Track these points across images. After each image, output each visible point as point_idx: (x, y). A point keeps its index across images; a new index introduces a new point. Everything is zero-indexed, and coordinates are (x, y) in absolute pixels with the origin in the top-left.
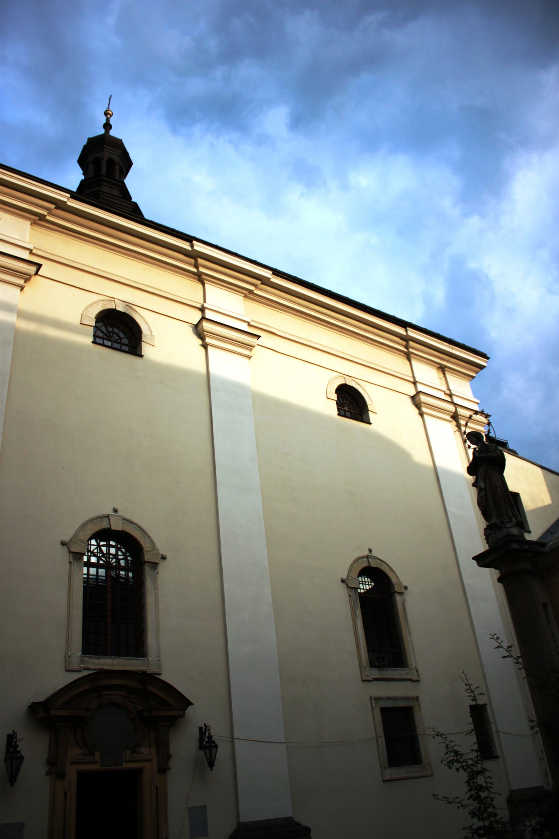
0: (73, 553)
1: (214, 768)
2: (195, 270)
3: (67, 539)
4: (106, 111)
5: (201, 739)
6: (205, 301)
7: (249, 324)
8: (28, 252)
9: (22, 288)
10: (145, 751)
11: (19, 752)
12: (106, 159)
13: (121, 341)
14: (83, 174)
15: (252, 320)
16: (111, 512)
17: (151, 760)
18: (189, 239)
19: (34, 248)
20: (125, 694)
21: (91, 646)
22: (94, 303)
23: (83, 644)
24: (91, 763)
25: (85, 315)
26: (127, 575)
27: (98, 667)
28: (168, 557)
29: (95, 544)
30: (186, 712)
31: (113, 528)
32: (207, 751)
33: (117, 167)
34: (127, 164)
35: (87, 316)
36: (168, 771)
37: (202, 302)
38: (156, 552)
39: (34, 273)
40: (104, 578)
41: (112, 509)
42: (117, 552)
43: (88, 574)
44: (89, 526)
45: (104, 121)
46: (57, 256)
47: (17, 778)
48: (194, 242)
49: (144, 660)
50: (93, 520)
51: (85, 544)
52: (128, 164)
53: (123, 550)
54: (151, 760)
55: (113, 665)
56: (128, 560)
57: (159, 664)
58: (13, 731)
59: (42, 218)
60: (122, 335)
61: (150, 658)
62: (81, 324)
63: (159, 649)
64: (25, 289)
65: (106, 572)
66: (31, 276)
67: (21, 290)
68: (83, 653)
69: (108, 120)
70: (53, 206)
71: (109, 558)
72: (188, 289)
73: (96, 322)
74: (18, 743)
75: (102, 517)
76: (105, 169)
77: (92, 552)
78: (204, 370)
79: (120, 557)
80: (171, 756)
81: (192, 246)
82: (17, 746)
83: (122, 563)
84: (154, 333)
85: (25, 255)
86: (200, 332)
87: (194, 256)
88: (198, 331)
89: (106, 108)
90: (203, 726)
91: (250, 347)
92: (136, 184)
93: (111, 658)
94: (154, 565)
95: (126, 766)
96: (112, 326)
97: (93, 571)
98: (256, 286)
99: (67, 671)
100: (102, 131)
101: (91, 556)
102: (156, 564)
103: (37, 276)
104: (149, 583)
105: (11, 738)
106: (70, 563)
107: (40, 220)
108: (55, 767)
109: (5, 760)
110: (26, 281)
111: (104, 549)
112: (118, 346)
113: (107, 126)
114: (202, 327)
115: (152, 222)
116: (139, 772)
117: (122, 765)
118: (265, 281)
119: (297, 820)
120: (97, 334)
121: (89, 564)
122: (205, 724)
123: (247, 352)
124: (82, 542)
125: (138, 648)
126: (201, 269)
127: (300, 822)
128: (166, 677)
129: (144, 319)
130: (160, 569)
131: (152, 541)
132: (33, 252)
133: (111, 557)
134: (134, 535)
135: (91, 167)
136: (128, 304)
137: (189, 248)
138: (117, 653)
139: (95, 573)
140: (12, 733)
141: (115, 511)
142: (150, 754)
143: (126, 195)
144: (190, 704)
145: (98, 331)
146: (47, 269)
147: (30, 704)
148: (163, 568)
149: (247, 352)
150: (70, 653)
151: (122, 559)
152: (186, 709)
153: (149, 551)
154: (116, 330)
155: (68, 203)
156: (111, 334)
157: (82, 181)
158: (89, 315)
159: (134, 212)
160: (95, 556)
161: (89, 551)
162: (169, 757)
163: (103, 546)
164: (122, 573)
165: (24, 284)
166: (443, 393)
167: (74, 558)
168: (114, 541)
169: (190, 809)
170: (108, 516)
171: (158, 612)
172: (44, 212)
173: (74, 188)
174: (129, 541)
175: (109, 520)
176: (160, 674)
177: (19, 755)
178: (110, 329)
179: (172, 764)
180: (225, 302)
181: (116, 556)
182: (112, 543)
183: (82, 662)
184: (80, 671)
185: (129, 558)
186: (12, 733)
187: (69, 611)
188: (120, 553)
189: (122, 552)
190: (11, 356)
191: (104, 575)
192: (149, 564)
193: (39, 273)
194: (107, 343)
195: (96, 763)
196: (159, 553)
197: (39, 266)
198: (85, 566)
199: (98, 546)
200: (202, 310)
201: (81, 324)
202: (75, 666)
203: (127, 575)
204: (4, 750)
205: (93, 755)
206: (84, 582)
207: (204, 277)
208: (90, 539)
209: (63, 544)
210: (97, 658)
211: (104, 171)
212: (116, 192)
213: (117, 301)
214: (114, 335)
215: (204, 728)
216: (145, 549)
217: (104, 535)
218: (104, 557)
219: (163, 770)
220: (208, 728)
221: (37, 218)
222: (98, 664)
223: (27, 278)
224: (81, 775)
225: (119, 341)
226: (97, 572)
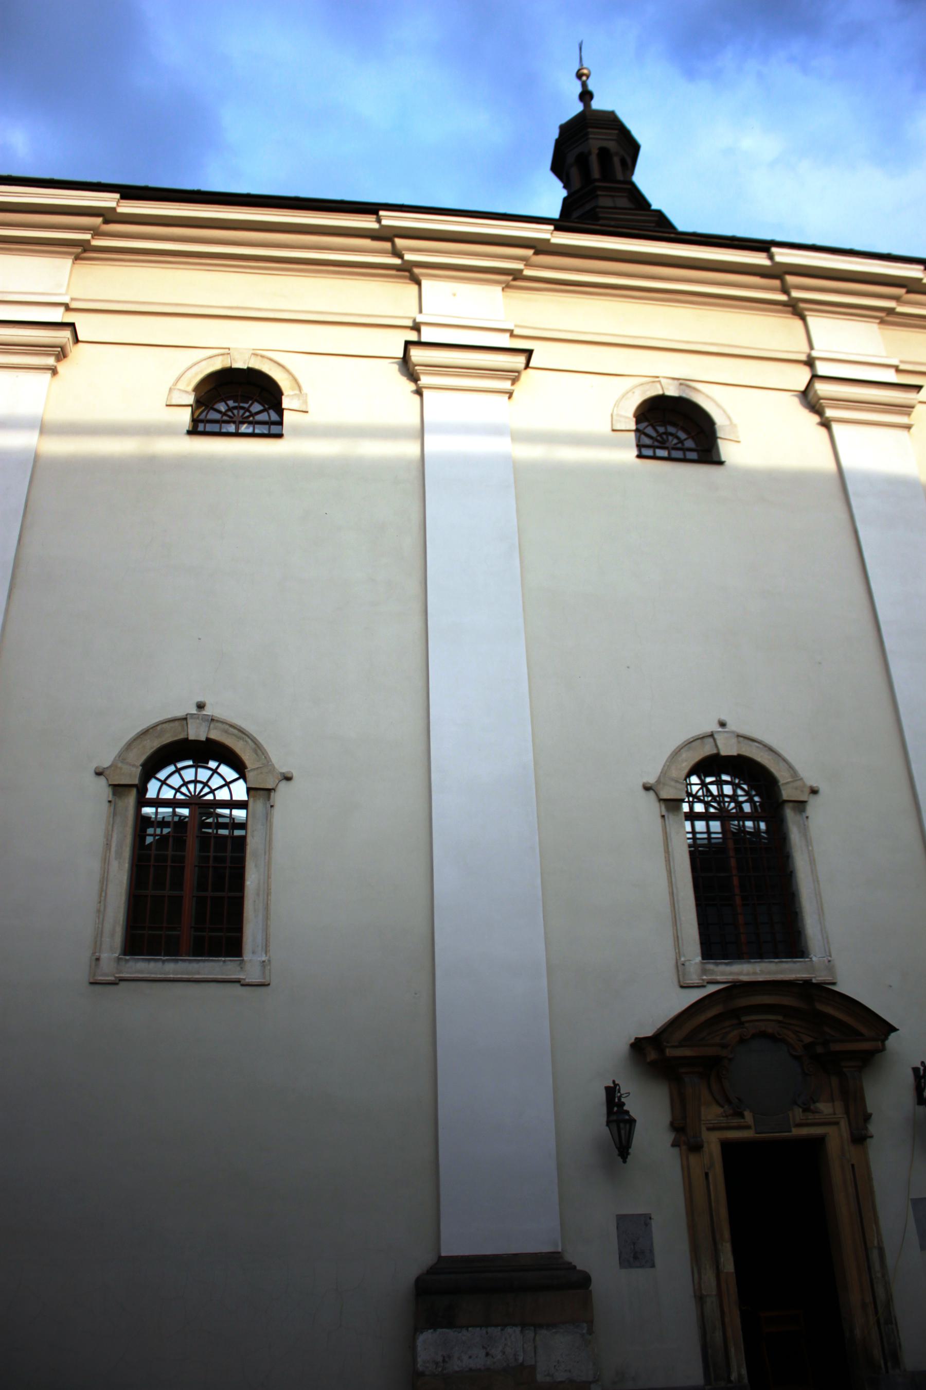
0: (665, 800)
2: (784, 298)
3: (651, 780)
4: (579, 70)
6: (811, 347)
7: (898, 370)
8: (508, 335)
9: (510, 394)
10: (825, 1108)
11: (627, 1112)
12: (595, 151)
13: (683, 444)
14: (565, 187)
15: (902, 362)
16: (716, 728)
17: (837, 1123)
18: (763, 246)
19: (516, 326)
20: (780, 1018)
21: (714, 946)
22: (627, 393)
23: (702, 943)
25: (618, 415)
26: (757, 828)
27: (730, 978)
28: (821, 791)
29: (698, 781)
30: (887, 1043)
31: (724, 753)
33: (616, 161)
34: (630, 148)
35: (621, 416)
36: (868, 1140)
37: (806, 348)
38: (799, 783)
39: (523, 366)
40: (720, 836)
41: (716, 722)
42: (734, 791)
43: (694, 832)
44: (684, 755)
45: (578, 89)
46: (559, 331)
47: (630, 1151)
48: (774, 250)
50: (689, 744)
51: (682, 783)
52: (631, 148)
53: (745, 787)
54: (837, 1123)
56: (755, 802)
57: (830, 966)
58: (614, 1082)
59: (517, 275)
60: (682, 435)
61: (814, 959)
62: (614, 430)
63: (828, 943)
64: (514, 395)
65: (723, 826)
66: (519, 372)
67: (510, 398)
68: (704, 957)
69: (584, 85)
70: (530, 252)
71: (724, 802)
72: (777, 333)
73: (637, 422)
74: (623, 1100)
75: (702, 738)
76: (597, 170)
77: (695, 796)
78: (832, 466)
79: (741, 799)
80: (870, 1115)
81: (771, 257)
82: (623, 1104)
83: (747, 808)
84: (735, 421)
85: (504, 341)
86: (813, 401)
87: (778, 273)
88: (810, 400)
89: (577, 67)
90: (919, 1065)
91: (906, 409)
92: (648, 178)
93: (749, 962)
94: (800, 806)
95: (796, 1132)
96: (664, 423)
97: (700, 826)
98: (897, 299)
99: (682, 987)
100: (579, 107)
101: (693, 802)
102: (803, 803)
103: (529, 370)
104: (795, 836)
105: (612, 1092)
106: (663, 816)
107: (515, 279)
108: (685, 1135)
109: (607, 1125)
110: (514, 381)
111: (714, 789)
112: (679, 454)
113: (586, 96)
114: (816, 392)
115: (694, 234)
116: (819, 1142)
117: (790, 1131)
118: (109, 216)
119: (569, 1257)
120: (642, 443)
121: (692, 816)
123: (903, 420)
124: (677, 781)
125: (789, 940)
126: (795, 294)
128: (845, 987)
129: (710, 400)
130: (810, 810)
131: (791, 767)
132: (515, 332)
133: (727, 799)
134: (759, 759)
135: (574, 172)
136: (683, 382)
137: (767, 263)
138: (759, 953)
139: (705, 830)
140: (612, 1085)
141: (722, 724)
142: (835, 1114)
143: (639, 200)
144: (893, 1029)
145: (643, 437)
146: (543, 354)
147: (633, 1041)
148: (815, 807)
149: (903, 420)
150: (683, 959)
151: (746, 801)
152: (886, 1038)
153: (788, 783)
154: (671, 429)
155: (554, 241)
156: (664, 437)
157: (565, 200)
158: (623, 413)
159: (659, 227)
160: (700, 801)
161: (689, 794)
162: (867, 1117)
163: (711, 783)
164: (749, 824)
165: (512, 388)
166: (892, 371)
167: (668, 809)
168: (727, 773)
170: (712, 735)
171: (818, 881)
172: (518, 263)
173: (555, 214)
174: (749, 771)
175: (715, 740)
176: (834, 984)
177: (627, 1117)
178: (661, 430)
179: (872, 1128)
180: (847, 341)
181: (734, 798)
182: (725, 777)
183: (704, 971)
184: (704, 986)
185: (756, 799)
186: (612, 1085)
187: (672, 894)
188: (740, 792)
189: (743, 789)
190: (515, 506)
191: (719, 830)
192: (791, 804)
193: (531, 365)
194: (661, 453)
195: (748, 1127)
196: (804, 785)
197: (529, 353)
198: (686, 820)
199: (704, 785)
200: (810, 362)
201: (614, 430)
202: (694, 979)
203: (757, 828)
204: (604, 1110)
205: (742, 1116)
206: (690, 846)
207: (802, 305)
208: (689, 775)
209: (647, 788)
210: (726, 964)
211: (596, 173)
212: (623, 202)
213: (663, 381)
214: (670, 438)
215: (922, 1068)
216: (782, 781)
217: (710, 766)
218: (715, 801)
219: (860, 1138)
221: (510, 278)
222: (731, 974)
223: (514, 376)
224: (727, 1147)
225: (679, 445)
226: (708, 826)
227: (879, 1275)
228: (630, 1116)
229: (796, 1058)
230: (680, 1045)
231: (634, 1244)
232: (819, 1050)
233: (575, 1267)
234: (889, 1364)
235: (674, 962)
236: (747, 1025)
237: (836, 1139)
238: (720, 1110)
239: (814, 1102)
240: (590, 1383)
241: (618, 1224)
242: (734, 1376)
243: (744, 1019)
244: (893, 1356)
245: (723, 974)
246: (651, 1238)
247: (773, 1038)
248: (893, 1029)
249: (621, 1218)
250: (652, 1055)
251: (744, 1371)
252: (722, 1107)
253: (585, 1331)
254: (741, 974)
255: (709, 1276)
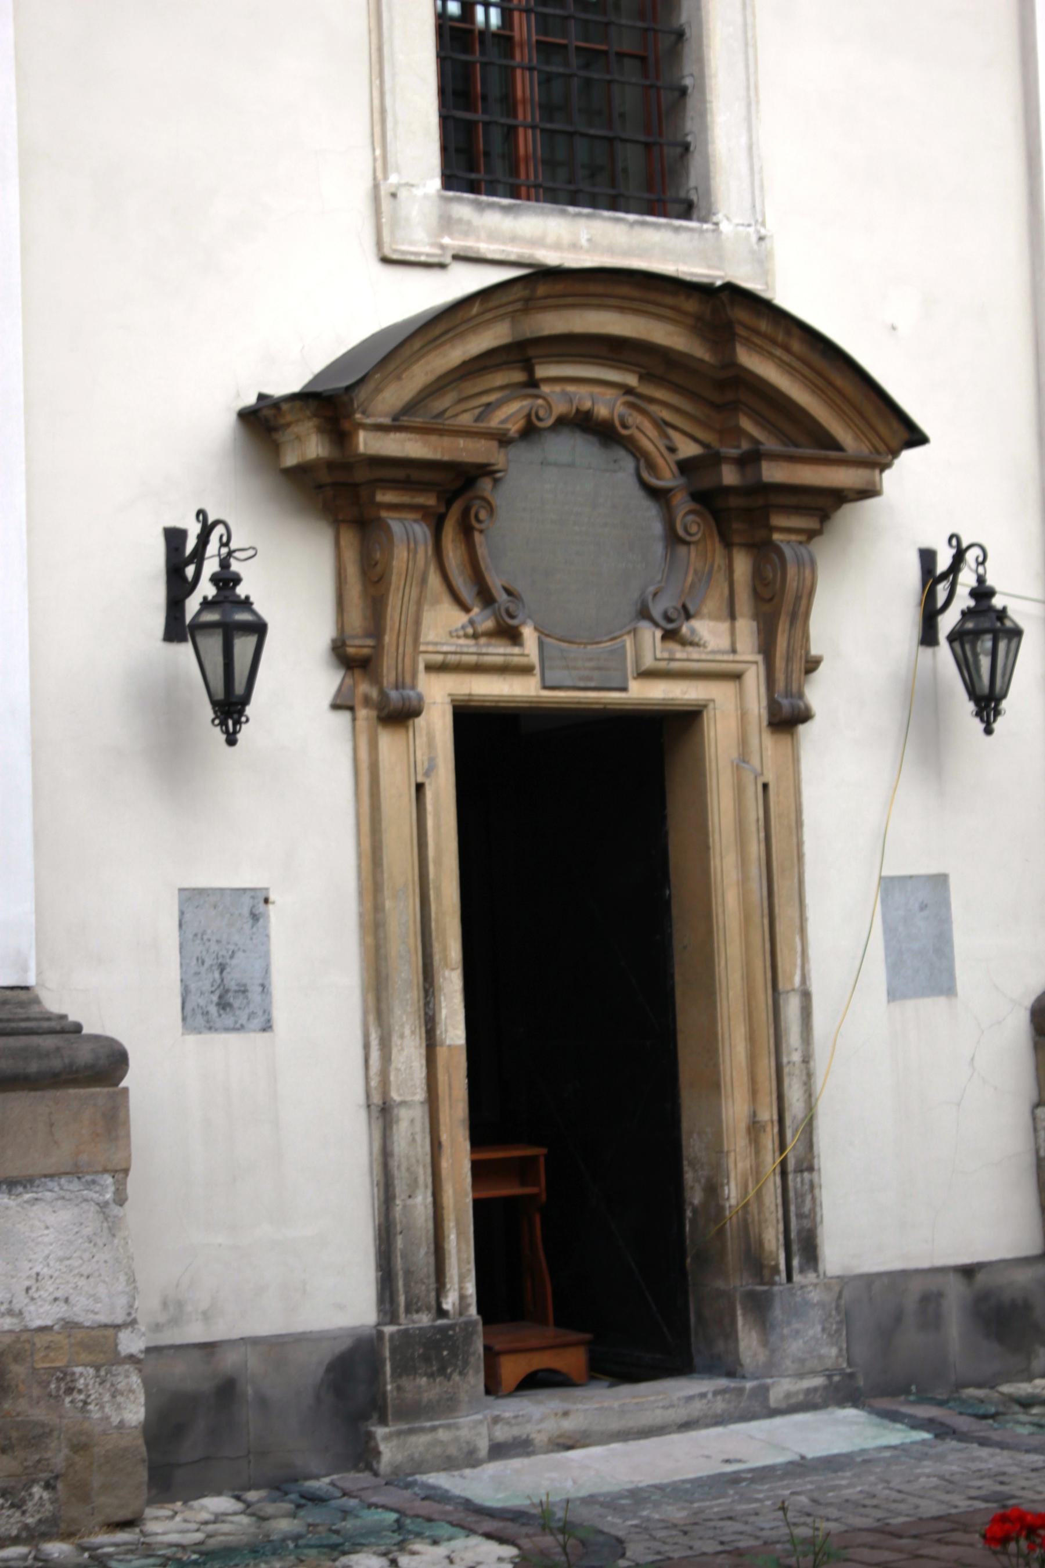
1: (998, 725)
5: (178, 587)
10: (710, 633)
11: (246, 604)
17: (737, 677)
20: (632, 380)
21: (475, 157)
24: (504, 670)
32: (213, 645)
49: (702, 232)
54: (737, 677)
55: (575, 246)
61: (725, 227)
68: (449, 181)
74: (235, 566)
82: (237, 580)
93: (564, 213)
99: (386, 261)
108: (368, 675)
116: (686, 720)
117: (624, 689)
119: (54, 1003)
122: (201, 514)
125: (657, 172)
127: (74, 1016)
142: (734, 651)
144: (916, 438)
147: (251, 400)
150: (393, 179)
169: (889, 885)
179: (818, 694)
183: (447, 224)
195: (526, 670)
202: (418, 241)
205: (513, 636)
210: (506, 209)
219: (787, 718)
220: (971, 556)
222: (514, 239)
224: (472, 722)
227: (796, 1057)
228: (254, 613)
229: (656, 494)
230: (396, 425)
231: (222, 968)
232: (729, 476)
233: (77, 1028)
234: (796, 1262)
235: (367, 184)
236: (545, 389)
237: (730, 719)
238: (460, 618)
239: (688, 616)
240: (118, 1327)
241: (182, 913)
242: (449, 1303)
243: (542, 371)
244: (805, 1246)
245: (493, 236)
246: (266, 955)
247: (604, 433)
248: (916, 438)
249: (192, 898)
250: (310, 446)
251: (471, 1289)
252: (467, 609)
253: (109, 1196)
254: (538, 242)
255: (409, 1055)
